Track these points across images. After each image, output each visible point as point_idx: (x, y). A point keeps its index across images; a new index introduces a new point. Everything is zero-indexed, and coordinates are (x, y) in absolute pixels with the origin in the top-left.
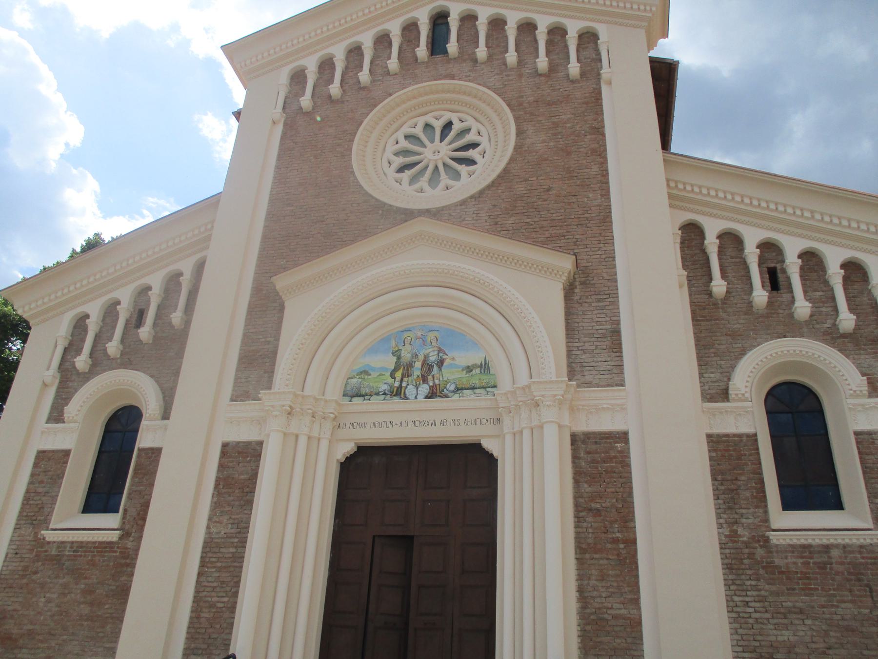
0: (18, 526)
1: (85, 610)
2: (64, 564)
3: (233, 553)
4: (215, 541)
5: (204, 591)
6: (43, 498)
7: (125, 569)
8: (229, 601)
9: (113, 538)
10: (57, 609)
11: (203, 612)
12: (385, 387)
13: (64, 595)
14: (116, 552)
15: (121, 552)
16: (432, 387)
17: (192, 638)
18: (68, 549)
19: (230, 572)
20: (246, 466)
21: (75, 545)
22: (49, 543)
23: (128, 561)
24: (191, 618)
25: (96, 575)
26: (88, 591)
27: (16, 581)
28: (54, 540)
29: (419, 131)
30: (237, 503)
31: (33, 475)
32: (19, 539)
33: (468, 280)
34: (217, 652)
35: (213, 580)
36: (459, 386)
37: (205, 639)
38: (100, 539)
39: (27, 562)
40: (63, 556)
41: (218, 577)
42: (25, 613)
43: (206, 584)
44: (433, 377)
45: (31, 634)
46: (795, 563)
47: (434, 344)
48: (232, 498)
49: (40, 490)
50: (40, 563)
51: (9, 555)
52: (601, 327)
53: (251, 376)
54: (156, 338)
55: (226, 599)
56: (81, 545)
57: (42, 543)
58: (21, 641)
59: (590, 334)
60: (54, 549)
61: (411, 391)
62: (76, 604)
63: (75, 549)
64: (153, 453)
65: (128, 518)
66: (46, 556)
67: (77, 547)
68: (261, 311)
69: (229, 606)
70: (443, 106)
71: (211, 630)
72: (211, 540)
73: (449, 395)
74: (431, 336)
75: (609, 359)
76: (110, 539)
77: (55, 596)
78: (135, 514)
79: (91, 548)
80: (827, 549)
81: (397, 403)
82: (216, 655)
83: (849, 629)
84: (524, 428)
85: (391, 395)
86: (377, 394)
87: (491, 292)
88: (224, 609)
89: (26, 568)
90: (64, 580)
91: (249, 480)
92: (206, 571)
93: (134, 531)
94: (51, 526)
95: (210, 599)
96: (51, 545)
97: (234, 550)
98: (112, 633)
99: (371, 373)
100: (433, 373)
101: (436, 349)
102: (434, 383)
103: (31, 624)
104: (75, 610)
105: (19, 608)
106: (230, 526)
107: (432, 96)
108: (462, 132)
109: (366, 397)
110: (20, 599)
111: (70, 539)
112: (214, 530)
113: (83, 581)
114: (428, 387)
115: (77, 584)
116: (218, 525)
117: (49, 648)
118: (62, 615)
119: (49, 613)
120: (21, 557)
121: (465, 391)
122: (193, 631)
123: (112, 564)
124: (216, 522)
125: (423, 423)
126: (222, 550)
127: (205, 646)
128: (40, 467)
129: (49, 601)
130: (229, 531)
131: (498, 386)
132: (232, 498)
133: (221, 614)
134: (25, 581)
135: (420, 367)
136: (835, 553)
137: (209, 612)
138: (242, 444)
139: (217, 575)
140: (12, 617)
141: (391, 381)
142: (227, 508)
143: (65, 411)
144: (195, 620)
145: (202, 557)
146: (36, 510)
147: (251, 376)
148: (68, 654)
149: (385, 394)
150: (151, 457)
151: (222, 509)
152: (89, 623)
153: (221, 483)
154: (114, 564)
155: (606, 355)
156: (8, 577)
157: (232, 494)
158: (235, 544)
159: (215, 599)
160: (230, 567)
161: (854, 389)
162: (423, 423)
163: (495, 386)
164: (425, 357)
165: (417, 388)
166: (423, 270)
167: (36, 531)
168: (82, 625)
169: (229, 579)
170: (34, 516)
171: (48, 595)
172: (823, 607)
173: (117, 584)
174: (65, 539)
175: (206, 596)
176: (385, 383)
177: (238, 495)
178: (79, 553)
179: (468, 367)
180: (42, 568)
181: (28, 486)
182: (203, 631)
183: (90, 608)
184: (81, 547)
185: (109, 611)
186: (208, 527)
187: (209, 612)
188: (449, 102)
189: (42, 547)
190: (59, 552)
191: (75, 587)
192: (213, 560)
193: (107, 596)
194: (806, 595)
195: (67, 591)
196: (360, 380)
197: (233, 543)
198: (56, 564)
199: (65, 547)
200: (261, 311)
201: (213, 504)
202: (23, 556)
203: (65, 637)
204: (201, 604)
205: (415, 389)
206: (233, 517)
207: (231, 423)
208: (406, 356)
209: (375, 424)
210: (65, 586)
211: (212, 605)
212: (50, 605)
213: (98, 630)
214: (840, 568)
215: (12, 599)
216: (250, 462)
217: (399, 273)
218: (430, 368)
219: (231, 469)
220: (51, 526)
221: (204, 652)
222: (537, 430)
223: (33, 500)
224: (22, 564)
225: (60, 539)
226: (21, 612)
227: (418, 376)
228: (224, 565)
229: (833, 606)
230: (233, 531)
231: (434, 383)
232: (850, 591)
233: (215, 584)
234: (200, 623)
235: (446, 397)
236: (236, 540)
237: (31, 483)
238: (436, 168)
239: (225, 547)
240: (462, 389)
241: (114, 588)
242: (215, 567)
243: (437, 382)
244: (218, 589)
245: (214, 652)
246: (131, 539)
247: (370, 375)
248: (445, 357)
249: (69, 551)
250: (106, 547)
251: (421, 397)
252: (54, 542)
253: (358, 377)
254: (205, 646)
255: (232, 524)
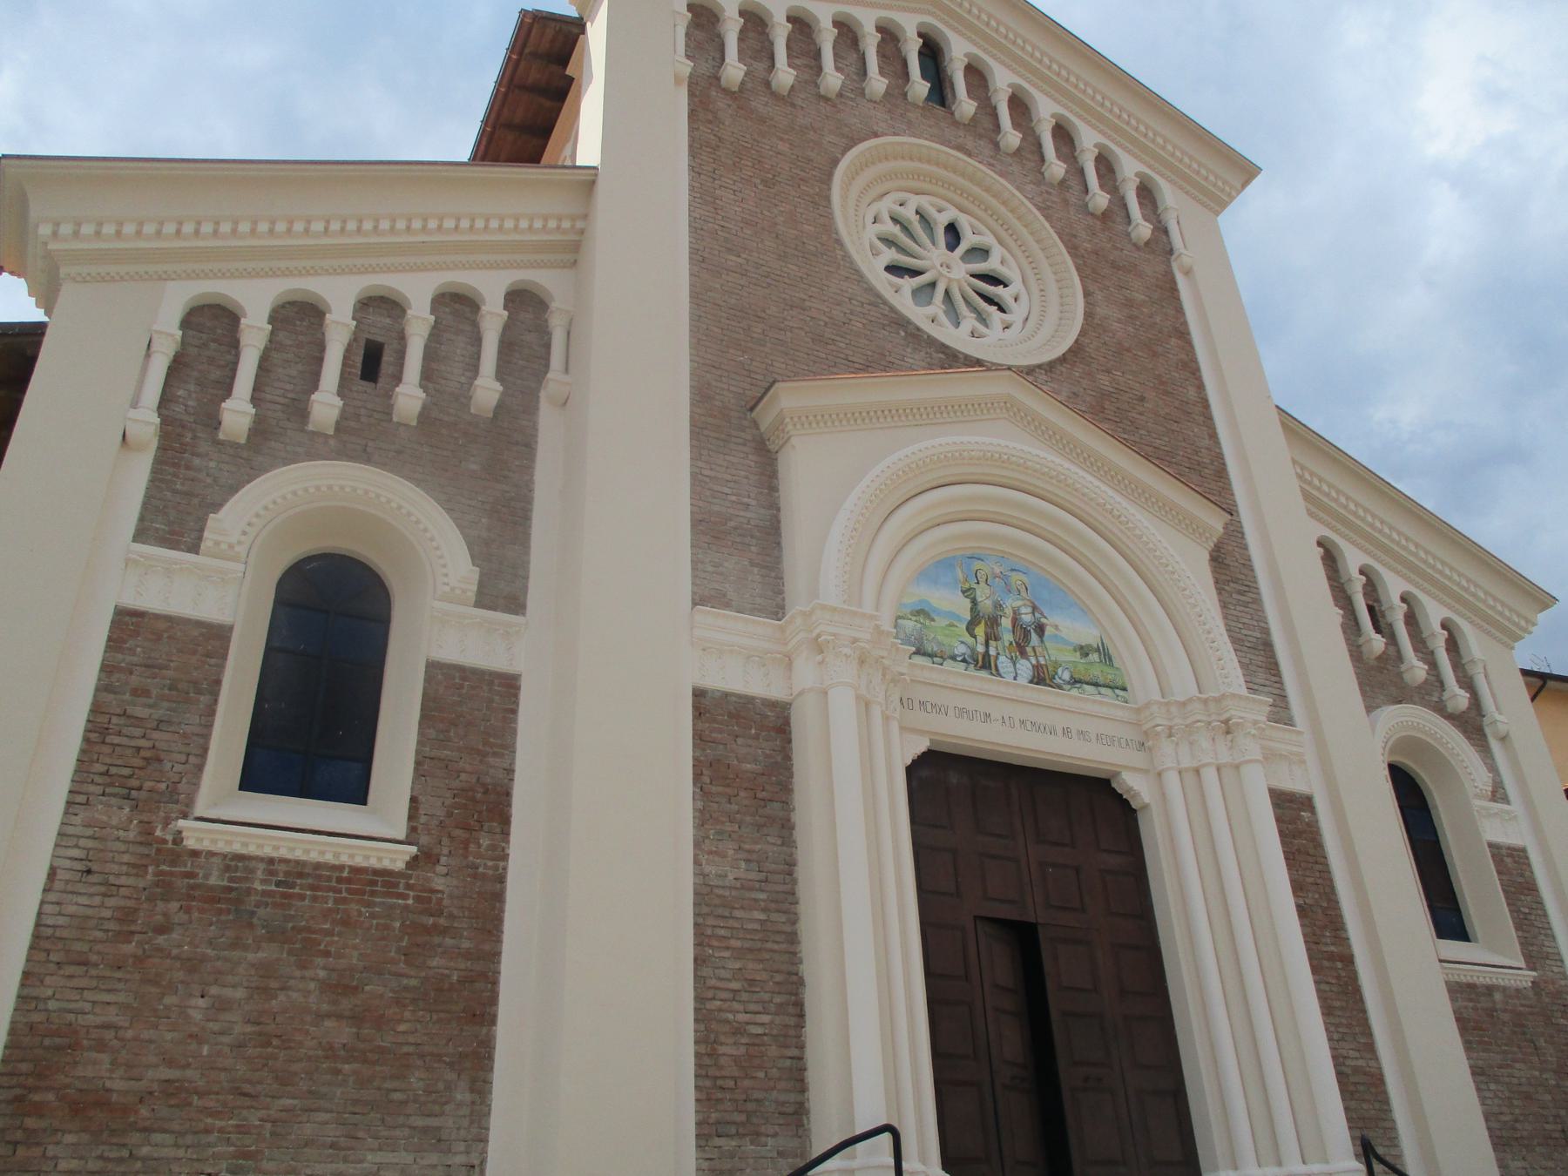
0: (81, 799)
1: (342, 1033)
2: (253, 913)
3: (762, 922)
4: (720, 892)
5: (714, 999)
6: (156, 735)
7: (437, 940)
8: (772, 1022)
9: (393, 861)
10: (249, 1029)
11: (722, 1044)
12: (961, 650)
13: (267, 993)
14: (404, 897)
15: (418, 899)
16: (1037, 668)
17: (709, 1100)
18: (259, 874)
19: (761, 961)
20: (750, 746)
21: (283, 867)
22: (195, 854)
23: (442, 921)
24: (698, 1055)
25: (355, 947)
26: (340, 987)
27: (99, 947)
28: (212, 848)
29: (942, 220)
30: (748, 819)
31: (107, 668)
32: (89, 832)
33: (1086, 499)
34: (771, 1130)
35: (728, 976)
36: (1076, 676)
37: (736, 1101)
38: (359, 861)
39: (125, 897)
40: (249, 891)
41: (740, 969)
42: (146, 1035)
43: (713, 982)
44: (1033, 648)
45: (173, 1092)
46: (1466, 1007)
47: (1023, 593)
48: (735, 807)
49: (139, 711)
50: (174, 905)
51: (61, 875)
52: (1250, 633)
53: (726, 564)
54: (424, 415)
55: (766, 1019)
56: (294, 873)
57: (176, 852)
58: (144, 1111)
59: (1239, 639)
60: (215, 873)
61: (1004, 663)
62: (308, 1018)
63: (281, 877)
64: (464, 679)
65: (423, 819)
66: (193, 887)
67: (287, 873)
68: (717, 439)
69: (775, 1032)
70: (950, 195)
71: (747, 1083)
72: (709, 889)
73: (1064, 686)
74: (1016, 578)
75: (1267, 683)
76: (386, 864)
77: (240, 994)
78: (441, 813)
79: (329, 879)
80: (1490, 990)
81: (980, 680)
82: (768, 1136)
83: (1528, 1097)
84: (1168, 769)
85: (976, 666)
86: (953, 658)
87: (1129, 534)
88: (765, 1038)
89: (126, 916)
90: (260, 955)
91: (763, 774)
92: (710, 956)
93: (445, 851)
94: (198, 812)
95: (730, 1016)
96: (203, 860)
97: (762, 917)
98: (428, 1092)
99: (936, 618)
100: (1032, 644)
101: (1028, 603)
102: (1038, 661)
103: (170, 1063)
104: (307, 1033)
105: (122, 1021)
106: (743, 864)
107: (933, 168)
108: (892, 242)
109: (936, 659)
110: (121, 998)
111: (267, 851)
112: (710, 869)
113: (320, 961)
114: (1029, 666)
115: (303, 966)
116: (716, 859)
117: (242, 1130)
118: (269, 1044)
119: (226, 1039)
120: (106, 883)
121: (1085, 686)
122: (708, 1083)
123: (397, 924)
124: (710, 853)
125: (1037, 727)
126: (738, 913)
127: (742, 1118)
128: (132, 651)
129: (222, 1006)
130: (741, 873)
131: (1128, 688)
132: (735, 807)
133: (763, 1049)
134: (129, 948)
135: (1010, 627)
136: (1498, 996)
137: (735, 1043)
138: (734, 699)
139: (738, 965)
140: (101, 1046)
141: (970, 640)
142: (728, 827)
143: (210, 523)
144: (707, 1061)
145: (696, 925)
146: (137, 762)
147: (726, 564)
148: (306, 1145)
149: (964, 661)
150: (462, 686)
151: (718, 827)
152: (355, 1066)
153: (704, 772)
154: (403, 924)
155: (1264, 676)
156: (65, 933)
157: (733, 799)
158: (762, 904)
159: (742, 1017)
160: (759, 950)
161: (1481, 787)
162: (1037, 727)
163: (1125, 689)
164: (1015, 613)
165: (1014, 664)
166: (1029, 464)
167: (145, 817)
168: (338, 1072)
169: (764, 976)
170: (130, 777)
171: (214, 990)
172: (1500, 1067)
173: (423, 974)
174: (252, 850)
175: (720, 1010)
176: (962, 642)
177: (746, 802)
178: (297, 890)
179: (1081, 648)
180: (183, 917)
181: (95, 696)
182: (731, 1083)
183: (354, 1030)
184: (301, 875)
185: (411, 1040)
186: (697, 862)
187: (735, 1043)
188: (952, 188)
189: (173, 863)
190: (231, 880)
191: (298, 973)
192: (722, 932)
193: (398, 1002)
194: (1484, 1051)
195: (274, 984)
196: (919, 625)
197: (756, 900)
198: (229, 912)
199: (252, 871)
200: (717, 439)
201: (697, 814)
202: (112, 879)
203: (288, 1102)
204: (714, 1026)
205: (1011, 665)
206: (747, 847)
207: (704, 650)
208: (986, 605)
209: (962, 712)
210: (266, 970)
211: (738, 1031)
212: (228, 1016)
213: (388, 1085)
214: (1506, 1017)
215: (88, 995)
216: (756, 737)
217: (992, 456)
218: (1026, 634)
219: (721, 747)
220: (199, 810)
221: (741, 1130)
222: (1230, 771)
223: (119, 734)
224: (111, 902)
225: (237, 848)
226: (130, 1034)
227: (1011, 643)
228: (747, 945)
229: (1508, 1066)
230: (753, 875)
231: (1038, 661)
232: (1519, 1047)
233: (735, 985)
234: (721, 1068)
235: (1059, 687)
236: (762, 896)
237: (102, 688)
238: (933, 285)
239: (742, 908)
240: (1080, 681)
241: (413, 982)
242: (727, 948)
243: (1042, 661)
244: (745, 996)
245: (763, 1129)
246: (440, 869)
247: (933, 620)
248: (1043, 620)
249: (263, 882)
250: (374, 883)
251: (1023, 680)
252: (211, 854)
253: (914, 618)
254: (742, 1118)
255: (748, 861)
